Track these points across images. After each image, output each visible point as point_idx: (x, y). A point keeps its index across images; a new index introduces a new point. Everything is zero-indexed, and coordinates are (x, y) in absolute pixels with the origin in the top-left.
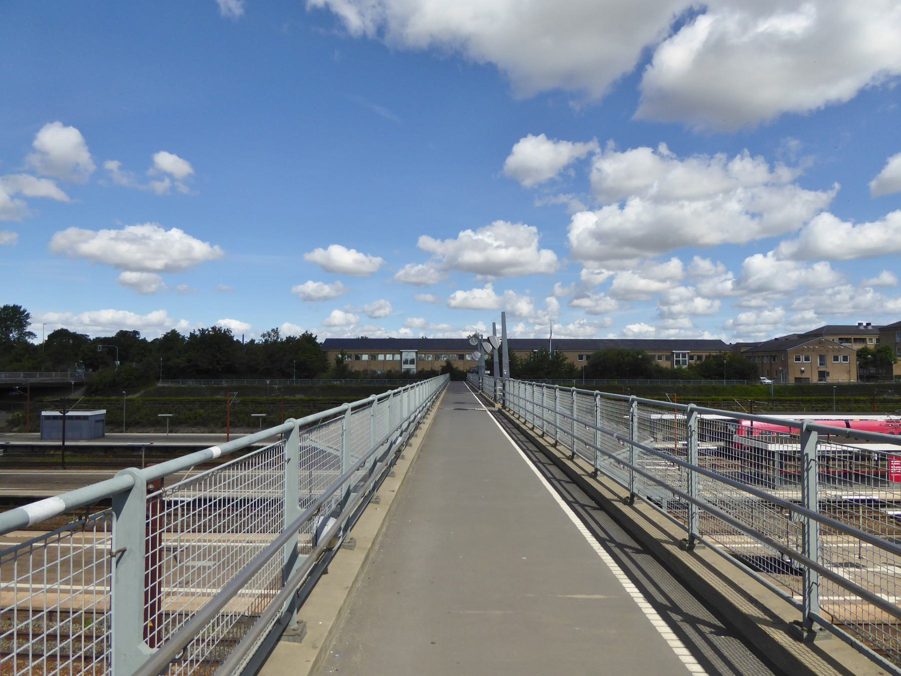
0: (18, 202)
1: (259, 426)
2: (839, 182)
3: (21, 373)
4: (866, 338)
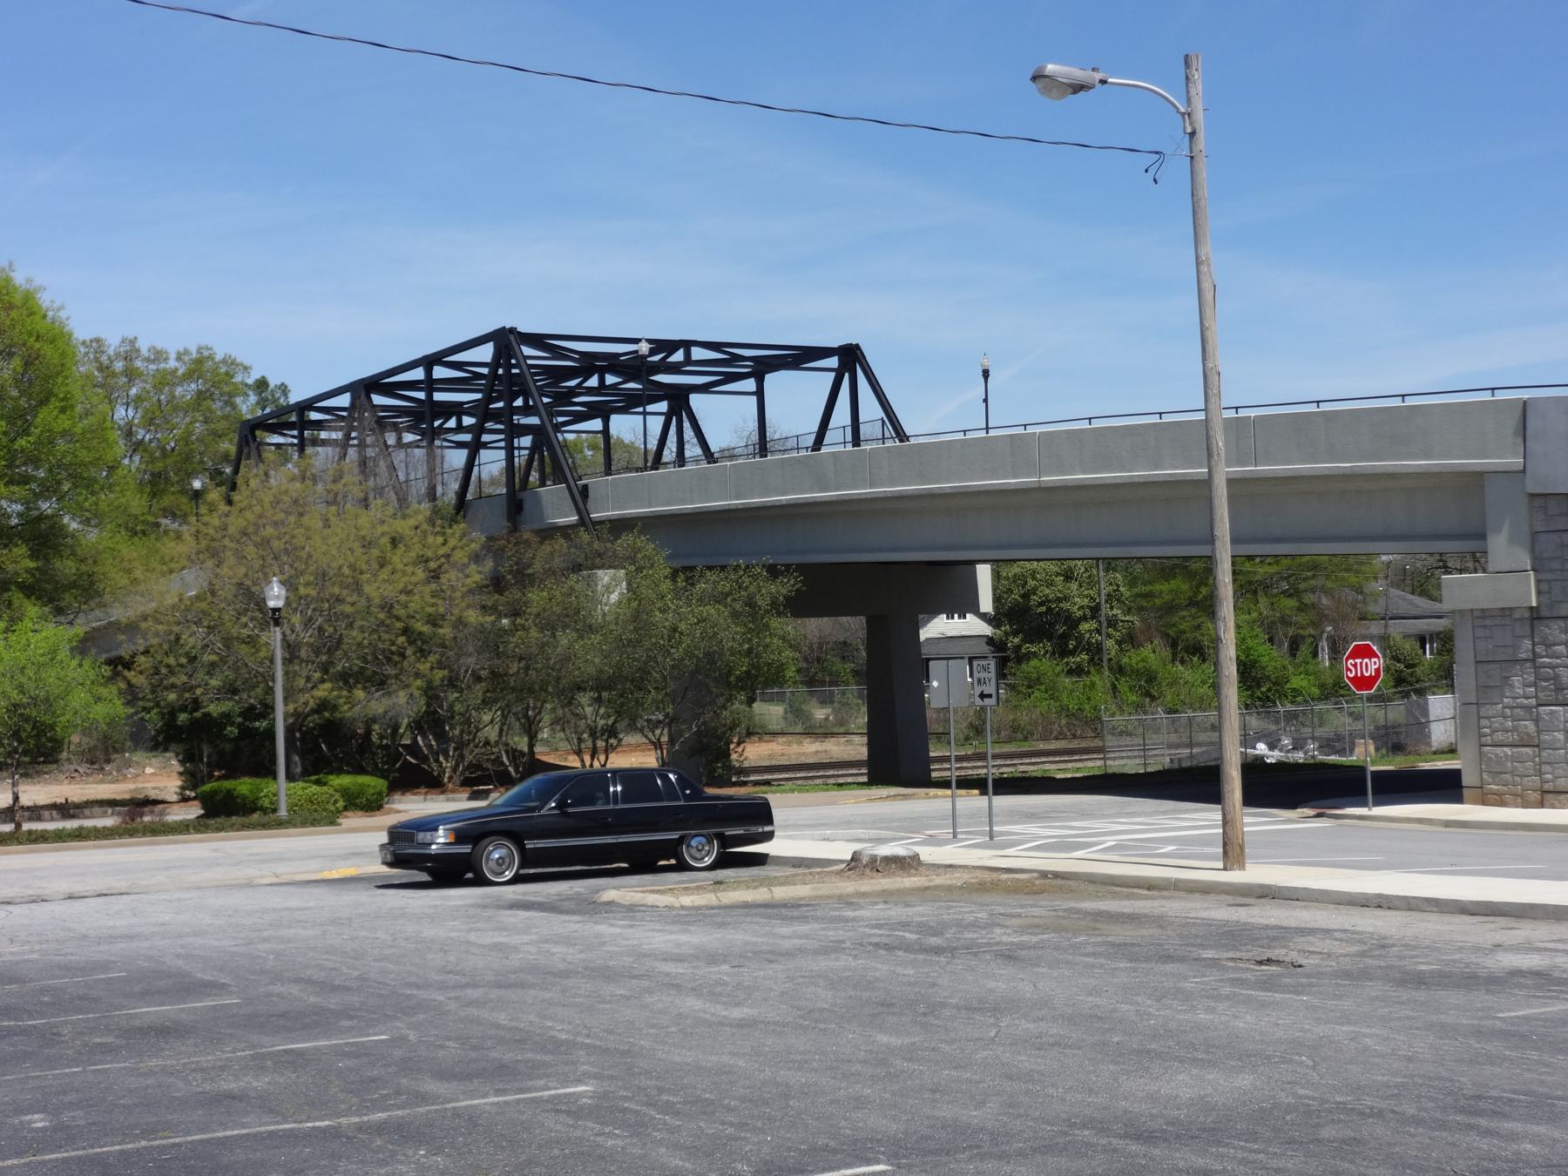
0: (113, 757)
1: (1365, 794)
4: (1231, 482)
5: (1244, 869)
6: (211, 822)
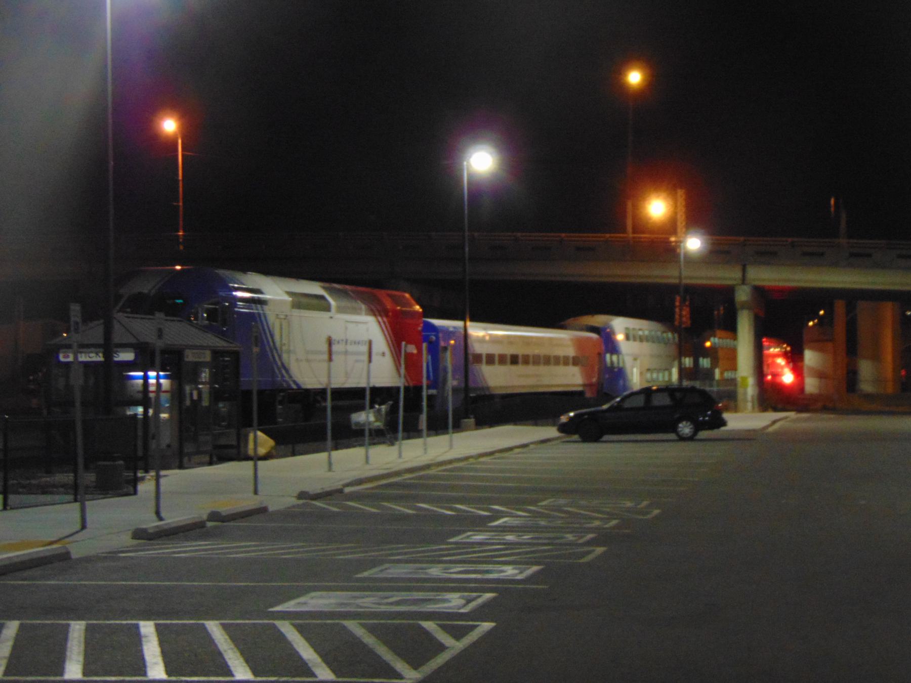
2: (707, 411)
5: (146, 637)
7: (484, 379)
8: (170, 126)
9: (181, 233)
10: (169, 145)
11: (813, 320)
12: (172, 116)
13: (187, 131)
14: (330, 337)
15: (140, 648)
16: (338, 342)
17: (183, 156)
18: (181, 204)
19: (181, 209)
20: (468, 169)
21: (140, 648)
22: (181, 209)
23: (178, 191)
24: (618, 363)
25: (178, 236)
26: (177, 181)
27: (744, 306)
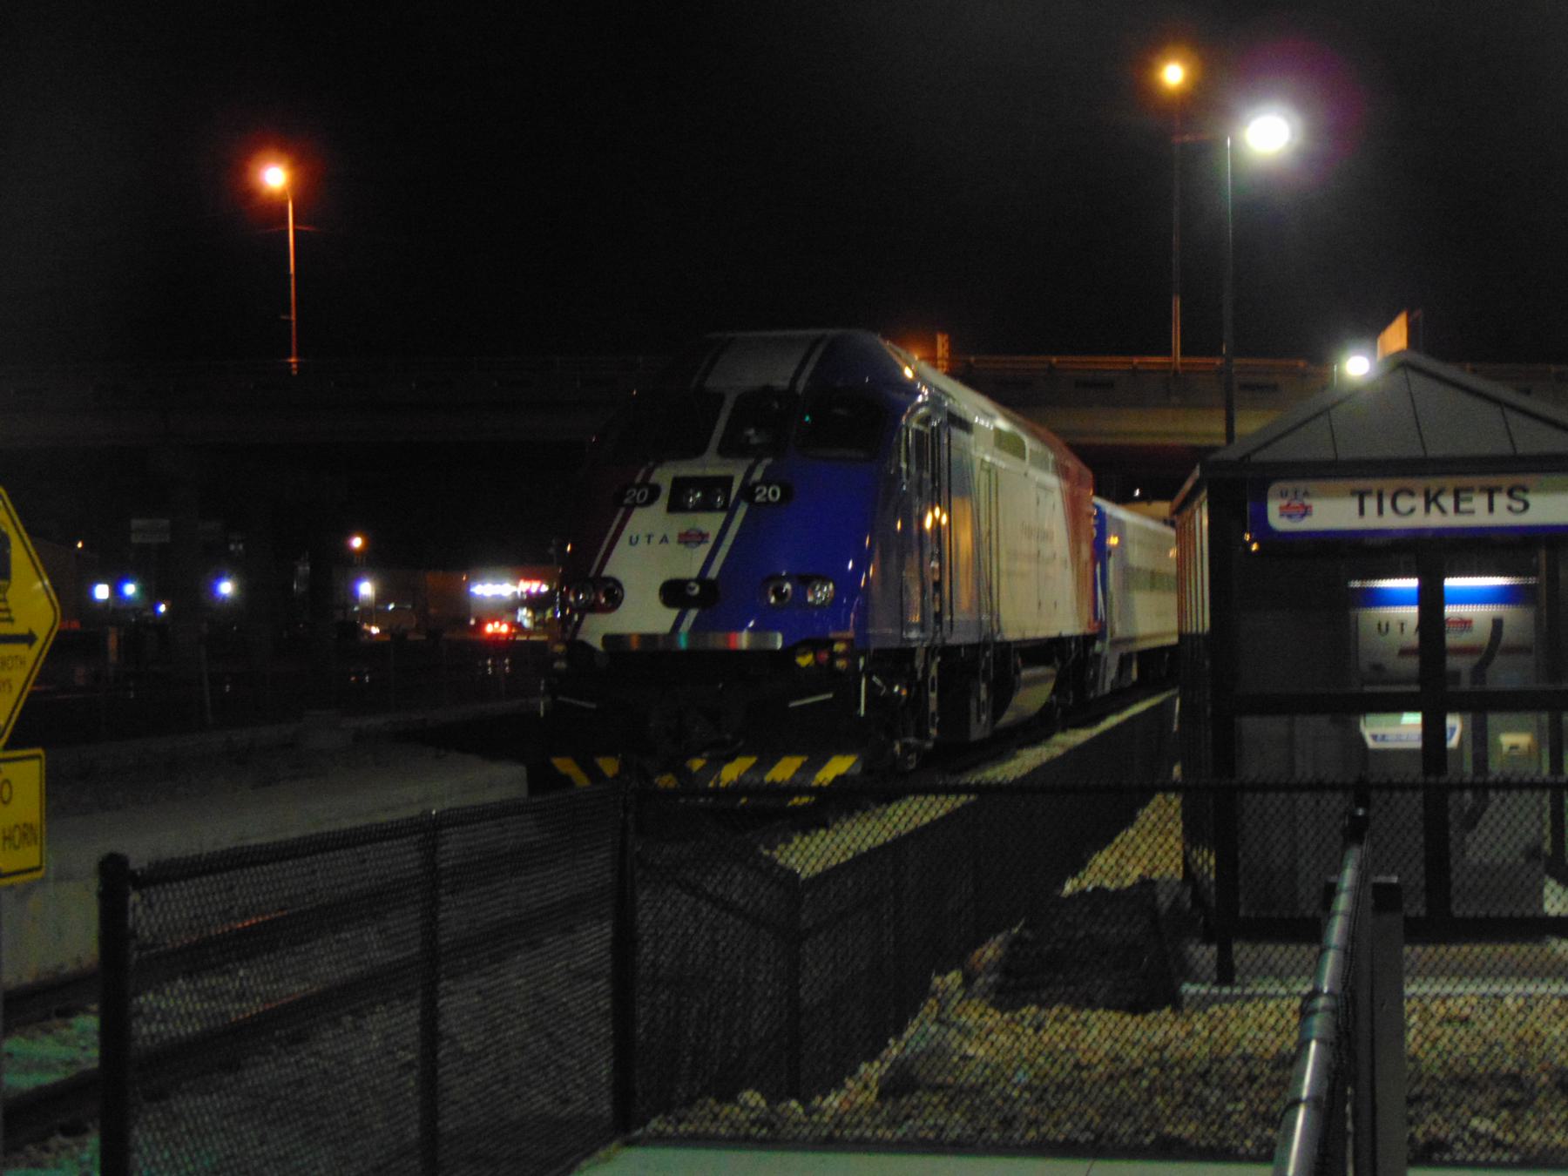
3: (1410, 990)
6: (1276, 1159)
7: (475, 807)
8: (275, 177)
9: (293, 360)
10: (272, 211)
11: (1371, 328)
12: (279, 161)
13: (305, 193)
14: (1068, 443)
15: (634, 639)
16: (664, 540)
17: (295, 230)
18: (293, 318)
19: (294, 324)
20: (1338, 377)
21: (634, 639)
22: (294, 324)
23: (290, 299)
24: (612, 1057)
25: (290, 364)
26: (289, 276)
27: (1220, 991)
